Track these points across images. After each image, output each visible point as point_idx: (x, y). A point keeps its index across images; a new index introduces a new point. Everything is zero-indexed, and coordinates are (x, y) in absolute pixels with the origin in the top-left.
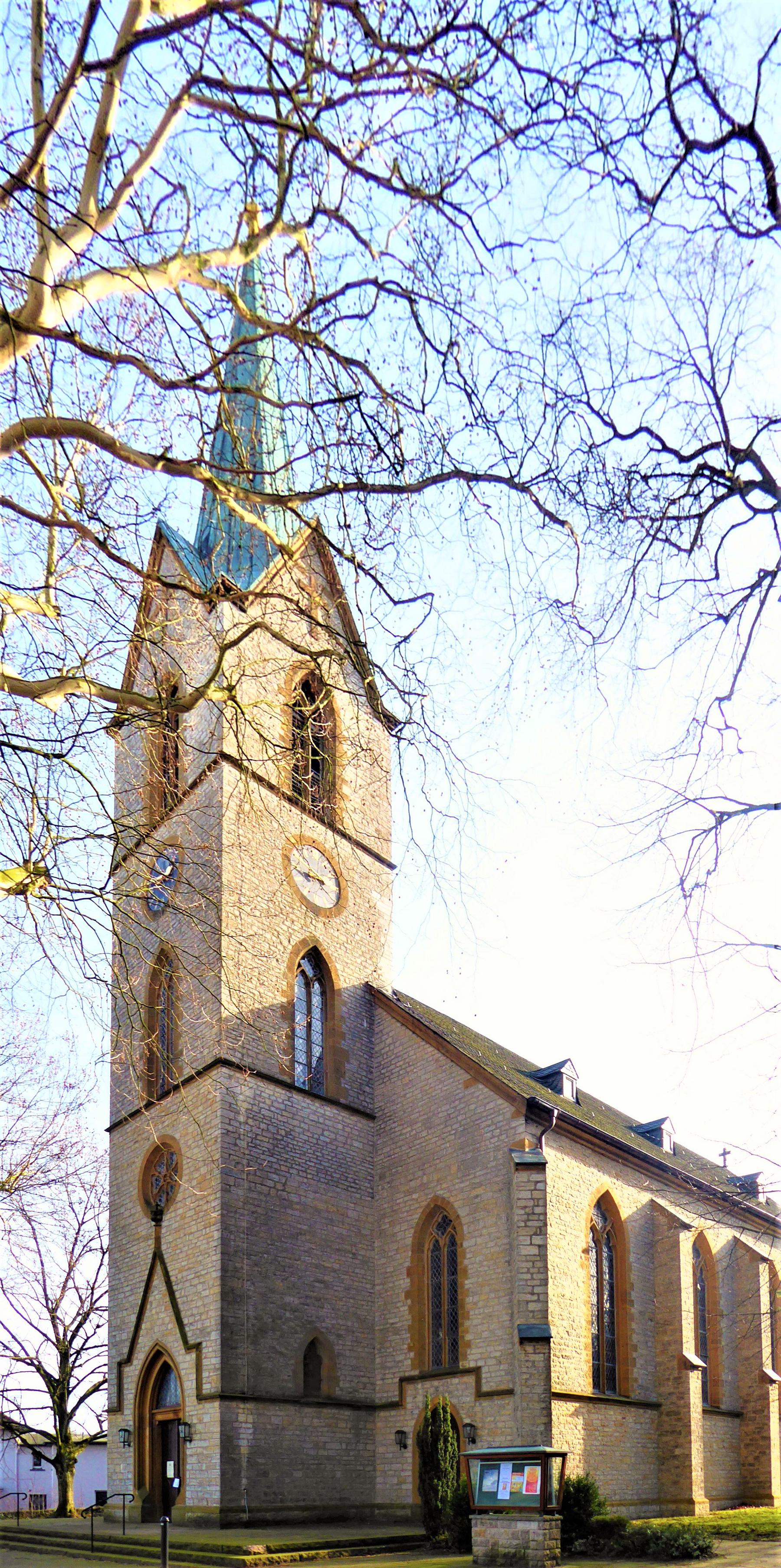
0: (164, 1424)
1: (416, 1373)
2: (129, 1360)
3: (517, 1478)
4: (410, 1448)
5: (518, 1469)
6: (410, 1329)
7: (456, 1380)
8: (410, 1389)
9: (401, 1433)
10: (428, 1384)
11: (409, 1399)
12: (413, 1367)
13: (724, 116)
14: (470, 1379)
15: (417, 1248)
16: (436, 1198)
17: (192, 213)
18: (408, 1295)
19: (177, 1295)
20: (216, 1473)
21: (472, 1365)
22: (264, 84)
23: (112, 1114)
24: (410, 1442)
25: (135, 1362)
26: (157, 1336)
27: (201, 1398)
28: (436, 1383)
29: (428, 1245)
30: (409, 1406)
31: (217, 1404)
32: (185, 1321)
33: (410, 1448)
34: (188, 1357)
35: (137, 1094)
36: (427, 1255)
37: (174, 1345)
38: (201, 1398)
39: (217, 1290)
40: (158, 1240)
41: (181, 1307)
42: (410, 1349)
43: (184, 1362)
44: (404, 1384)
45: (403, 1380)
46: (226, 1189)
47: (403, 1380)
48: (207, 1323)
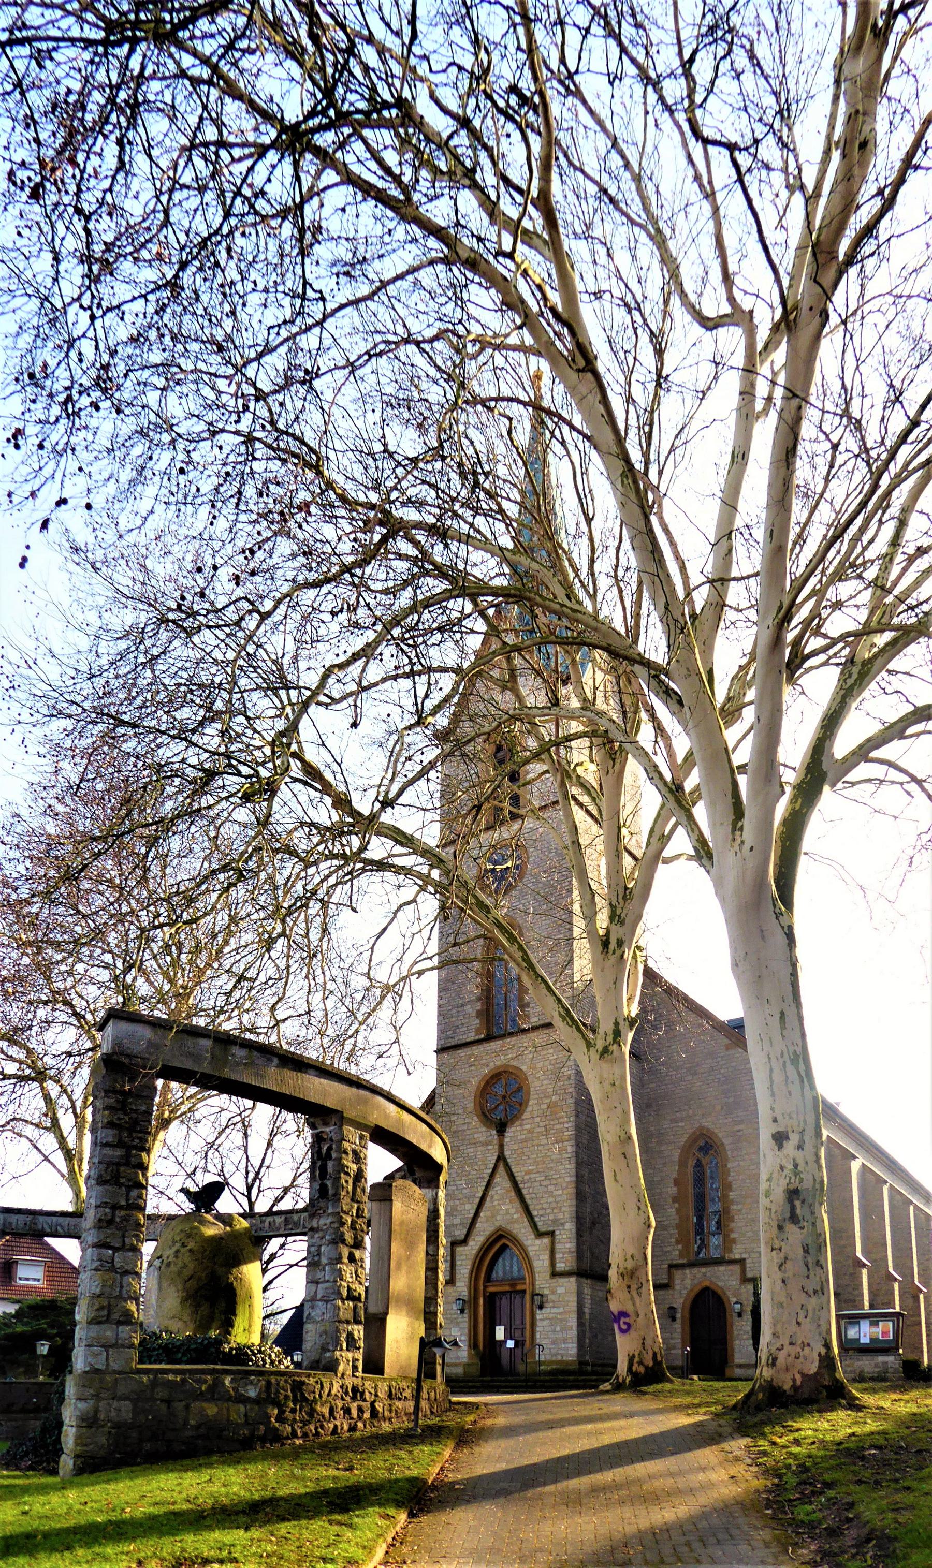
0: (493, 1295)
1: (684, 1261)
2: (464, 1242)
3: (874, 1330)
4: (679, 1320)
5: (875, 1324)
6: (678, 1226)
7: (722, 1268)
8: (678, 1274)
9: (672, 1309)
10: (695, 1270)
11: (677, 1282)
12: (681, 1256)
13: (731, 300)
14: (737, 1268)
15: (682, 1163)
16: (701, 1128)
17: (205, 115)
18: (675, 1200)
19: (524, 1192)
20: (574, 1333)
21: (737, 1257)
22: (694, 582)
23: (439, 1039)
24: (679, 1316)
25: (471, 1243)
26: (500, 1221)
27: (555, 1274)
28: (703, 1270)
29: (691, 1162)
30: (677, 1287)
31: (573, 1279)
32: (535, 1213)
33: (679, 1320)
34: (538, 1242)
35: (471, 1029)
36: (690, 1170)
37: (522, 1231)
38: (555, 1274)
39: (572, 1190)
40: (501, 1147)
41: (529, 1202)
42: (678, 1242)
43: (536, 1248)
44: (673, 1270)
45: (671, 1266)
46: (577, 1116)
47: (671, 1266)
48: (561, 1216)
